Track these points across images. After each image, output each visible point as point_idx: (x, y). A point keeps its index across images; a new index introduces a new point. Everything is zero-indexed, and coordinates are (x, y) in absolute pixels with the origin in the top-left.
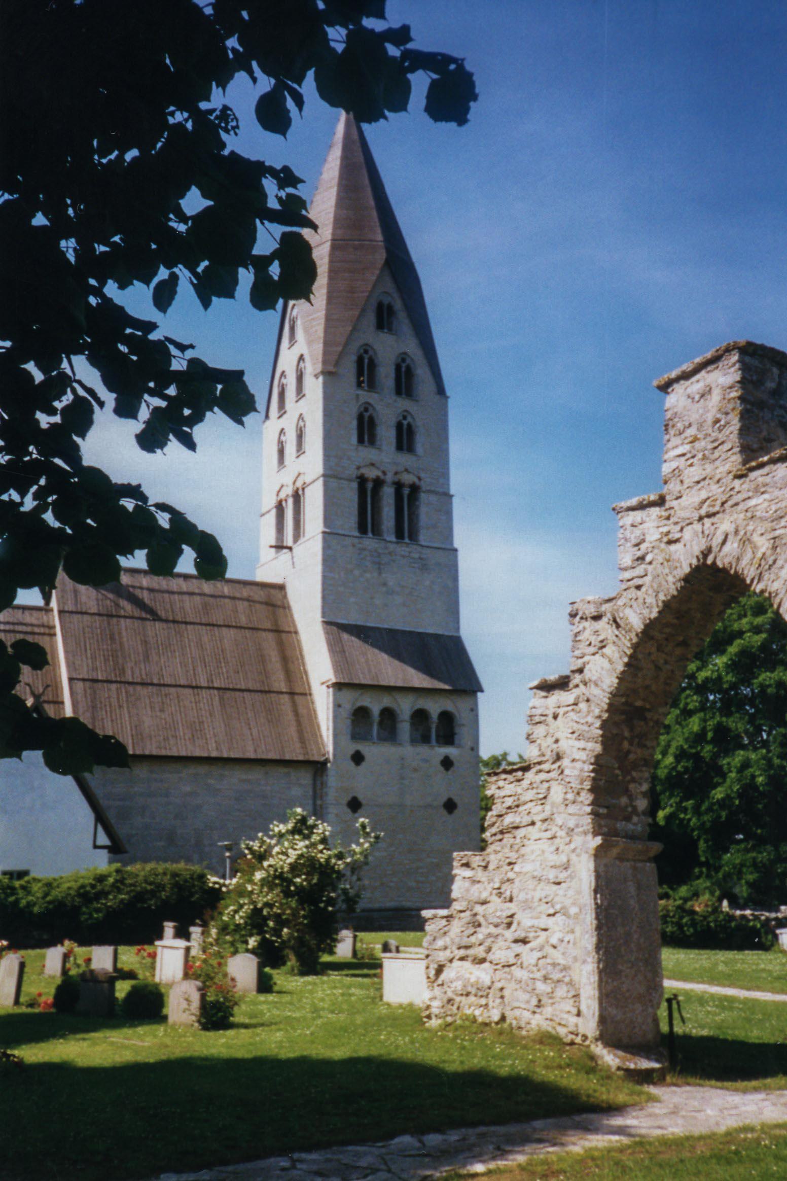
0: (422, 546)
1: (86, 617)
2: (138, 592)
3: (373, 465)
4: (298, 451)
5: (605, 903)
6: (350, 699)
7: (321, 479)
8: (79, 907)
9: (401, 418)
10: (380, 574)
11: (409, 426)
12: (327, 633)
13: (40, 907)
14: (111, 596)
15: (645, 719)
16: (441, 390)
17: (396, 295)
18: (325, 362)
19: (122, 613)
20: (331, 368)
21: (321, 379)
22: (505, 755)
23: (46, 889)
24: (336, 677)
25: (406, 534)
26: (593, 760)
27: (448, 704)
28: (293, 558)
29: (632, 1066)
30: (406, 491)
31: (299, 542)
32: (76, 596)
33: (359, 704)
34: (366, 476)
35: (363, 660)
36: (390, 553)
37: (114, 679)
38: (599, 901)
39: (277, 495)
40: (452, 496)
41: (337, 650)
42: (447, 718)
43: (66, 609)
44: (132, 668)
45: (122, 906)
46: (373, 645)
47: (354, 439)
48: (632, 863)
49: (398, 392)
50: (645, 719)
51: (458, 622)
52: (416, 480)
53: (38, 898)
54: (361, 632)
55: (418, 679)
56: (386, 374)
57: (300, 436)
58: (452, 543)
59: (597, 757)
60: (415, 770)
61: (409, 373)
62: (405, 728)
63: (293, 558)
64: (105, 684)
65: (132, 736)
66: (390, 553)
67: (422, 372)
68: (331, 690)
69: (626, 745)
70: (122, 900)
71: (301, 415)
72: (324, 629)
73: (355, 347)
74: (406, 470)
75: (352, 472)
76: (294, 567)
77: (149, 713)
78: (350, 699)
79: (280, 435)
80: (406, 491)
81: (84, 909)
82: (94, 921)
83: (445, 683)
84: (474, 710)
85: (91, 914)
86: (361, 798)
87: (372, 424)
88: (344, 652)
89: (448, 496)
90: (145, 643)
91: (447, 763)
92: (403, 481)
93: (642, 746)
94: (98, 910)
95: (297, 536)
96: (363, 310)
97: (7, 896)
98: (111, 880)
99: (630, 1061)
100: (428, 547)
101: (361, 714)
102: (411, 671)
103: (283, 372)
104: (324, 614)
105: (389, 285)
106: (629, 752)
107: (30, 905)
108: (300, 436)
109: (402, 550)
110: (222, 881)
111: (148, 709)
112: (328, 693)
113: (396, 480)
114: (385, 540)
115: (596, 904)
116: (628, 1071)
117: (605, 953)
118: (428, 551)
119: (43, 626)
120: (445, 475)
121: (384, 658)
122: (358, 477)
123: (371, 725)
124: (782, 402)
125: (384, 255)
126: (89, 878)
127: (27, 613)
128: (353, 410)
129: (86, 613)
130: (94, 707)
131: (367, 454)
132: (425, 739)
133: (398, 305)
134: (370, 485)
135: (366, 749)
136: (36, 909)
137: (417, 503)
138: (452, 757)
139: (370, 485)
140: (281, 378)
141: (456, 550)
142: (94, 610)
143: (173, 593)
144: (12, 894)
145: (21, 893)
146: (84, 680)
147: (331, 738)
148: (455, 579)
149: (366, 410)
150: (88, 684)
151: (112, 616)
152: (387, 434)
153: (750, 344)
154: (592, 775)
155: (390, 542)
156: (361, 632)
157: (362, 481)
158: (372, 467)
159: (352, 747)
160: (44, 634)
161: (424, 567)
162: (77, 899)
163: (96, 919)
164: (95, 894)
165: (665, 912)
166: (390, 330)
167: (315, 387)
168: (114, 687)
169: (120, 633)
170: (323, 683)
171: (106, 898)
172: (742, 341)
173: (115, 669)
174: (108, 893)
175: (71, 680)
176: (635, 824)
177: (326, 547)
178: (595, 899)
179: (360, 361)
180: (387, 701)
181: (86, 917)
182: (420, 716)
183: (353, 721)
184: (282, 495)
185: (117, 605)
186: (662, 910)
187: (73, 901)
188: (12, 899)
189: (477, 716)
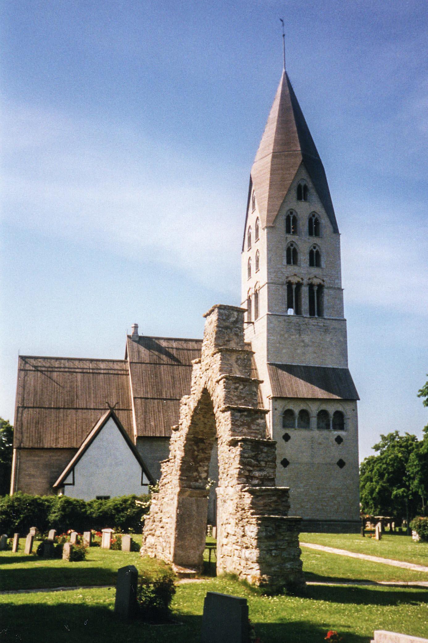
0: (325, 319)
1: (143, 365)
2: (170, 350)
3: (295, 275)
4: (257, 269)
5: (181, 513)
6: (281, 405)
7: (266, 285)
8: (114, 515)
9: (312, 248)
10: (300, 335)
11: (317, 252)
12: (269, 370)
13: (96, 515)
14: (157, 353)
15: (204, 443)
16: (336, 231)
17: (309, 180)
18: (268, 221)
19: (162, 362)
20: (271, 224)
21: (266, 230)
22: (397, 432)
23: (99, 506)
24: (273, 394)
25: (316, 313)
26: (181, 459)
27: (339, 407)
28: (254, 328)
29: (182, 572)
30: (316, 288)
31: (258, 319)
32: (139, 354)
33: (286, 408)
34: (292, 281)
35: (289, 384)
36: (306, 324)
37: (156, 397)
38: (178, 512)
39: (248, 293)
40: (342, 290)
41: (275, 379)
42: (339, 415)
43: (134, 361)
44: (166, 391)
45: (134, 515)
46: (295, 375)
47: (285, 261)
48: (196, 498)
49: (311, 234)
50: (204, 443)
51: (347, 361)
52: (321, 282)
53: (95, 510)
54: (290, 369)
55: (321, 393)
56: (303, 225)
57: (257, 261)
58: (343, 316)
59: (183, 458)
60: (320, 444)
61: (317, 223)
62: (314, 421)
63: (254, 328)
64: (152, 400)
65: (164, 427)
66: (306, 324)
67: (324, 221)
68: (271, 401)
69: (196, 453)
70: (134, 512)
71: (258, 250)
72: (268, 367)
73: (284, 212)
74: (316, 277)
75: (284, 280)
76: (255, 333)
77: (174, 415)
78: (281, 405)
79: (249, 260)
80: (316, 288)
81: (116, 516)
82: (121, 522)
83: (339, 396)
84: (355, 410)
85: (119, 518)
86: (288, 459)
87: (295, 252)
88: (279, 380)
89: (341, 290)
90: (173, 378)
91: (339, 440)
92: (313, 283)
93: (204, 453)
94: (123, 517)
95: (257, 316)
96: (289, 190)
97: (81, 509)
98: (129, 502)
99: (182, 570)
100: (329, 319)
101: (288, 414)
102: (317, 389)
103: (250, 226)
104: (268, 360)
105: (304, 174)
106: (198, 455)
107: (91, 513)
108: (257, 261)
109: (313, 322)
110: (142, 503)
111: (174, 413)
112: (269, 402)
113: (310, 283)
114: (303, 317)
115: (177, 513)
116: (180, 573)
117: (178, 532)
118: (328, 322)
119: (123, 370)
120: (339, 278)
121: (301, 382)
122: (287, 283)
123: (294, 420)
124: (237, 326)
125: (301, 159)
126: (119, 501)
127: (115, 363)
128: (284, 246)
129: (144, 363)
130: (146, 412)
131: (292, 269)
132: (327, 427)
133: (310, 185)
134: (294, 287)
135: (290, 432)
136: (94, 515)
137: (323, 295)
138: (342, 437)
139: (294, 287)
140: (249, 229)
141: (346, 320)
142: (147, 361)
143: (189, 350)
144: (84, 508)
145: (88, 507)
146: (141, 398)
147: (271, 427)
148: (345, 336)
149: (292, 245)
150: (143, 400)
151: (156, 364)
152: (304, 258)
153: (221, 306)
154: (181, 464)
155: (306, 317)
156: (290, 369)
157: (289, 284)
158: (295, 277)
159: (283, 432)
160: (123, 374)
161: (326, 330)
162: (113, 511)
163: (122, 521)
164: (122, 508)
165: (425, 524)
166: (306, 200)
167: (263, 234)
168: (156, 401)
169: (160, 373)
170: (267, 397)
171: (127, 511)
172: (219, 304)
173: (157, 392)
174: (128, 508)
175: (135, 398)
176: (200, 483)
177: (269, 322)
178: (177, 511)
179: (288, 219)
180: (303, 406)
181: (117, 519)
182: (323, 414)
183: (284, 418)
184: (250, 293)
185: (160, 358)
186: (423, 523)
187: (112, 512)
188: (83, 510)
189: (357, 413)
